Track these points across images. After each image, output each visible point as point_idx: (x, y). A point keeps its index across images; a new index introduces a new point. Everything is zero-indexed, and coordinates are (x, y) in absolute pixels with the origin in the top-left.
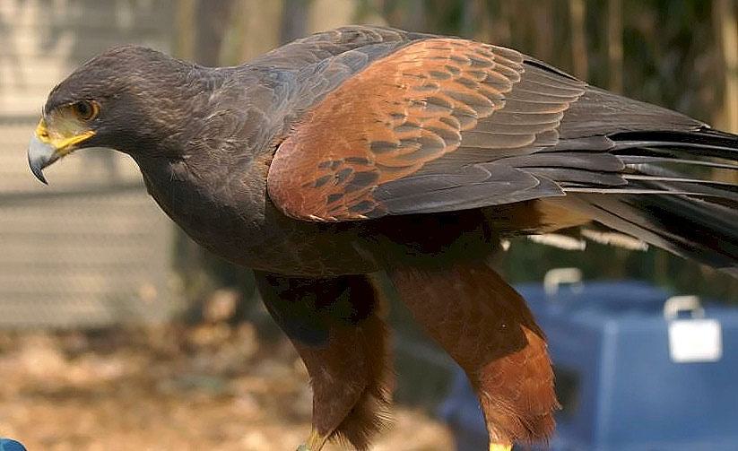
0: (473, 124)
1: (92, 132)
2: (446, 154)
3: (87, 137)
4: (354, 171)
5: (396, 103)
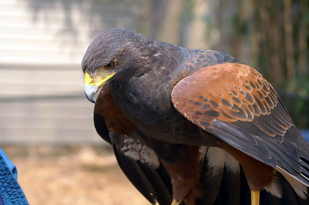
0: (258, 115)
1: (114, 73)
2: (246, 121)
3: (112, 76)
4: (211, 108)
5: (236, 87)
